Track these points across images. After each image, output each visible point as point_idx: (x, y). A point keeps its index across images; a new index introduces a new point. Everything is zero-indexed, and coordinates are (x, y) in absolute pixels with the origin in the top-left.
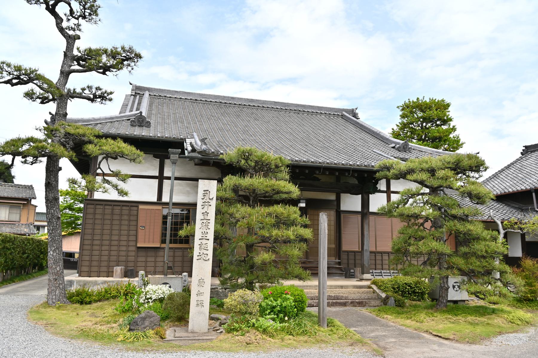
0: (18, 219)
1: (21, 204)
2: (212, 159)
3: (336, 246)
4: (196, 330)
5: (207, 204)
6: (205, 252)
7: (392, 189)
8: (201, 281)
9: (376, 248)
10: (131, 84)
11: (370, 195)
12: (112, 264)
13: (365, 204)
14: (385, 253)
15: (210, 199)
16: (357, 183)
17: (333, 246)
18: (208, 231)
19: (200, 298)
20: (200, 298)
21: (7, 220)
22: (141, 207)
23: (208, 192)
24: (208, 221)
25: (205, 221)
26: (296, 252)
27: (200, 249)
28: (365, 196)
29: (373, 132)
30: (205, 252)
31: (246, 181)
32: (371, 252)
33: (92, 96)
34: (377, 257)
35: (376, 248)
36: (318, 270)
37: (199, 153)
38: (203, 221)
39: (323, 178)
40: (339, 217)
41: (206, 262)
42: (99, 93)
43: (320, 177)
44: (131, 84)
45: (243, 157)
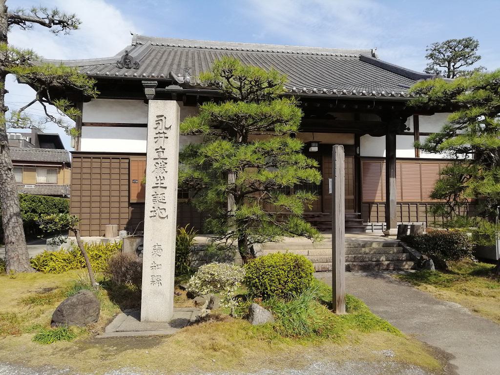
0: (55, 182)
1: (57, 167)
2: (197, 92)
3: (355, 197)
4: (151, 318)
5: (162, 135)
6: (162, 206)
7: (421, 130)
8: (157, 247)
9: (402, 198)
10: (132, 34)
11: (397, 136)
12: (103, 222)
13: (391, 147)
14: (412, 203)
15: (166, 129)
16: (381, 121)
17: (352, 197)
18: (165, 175)
19: (158, 272)
20: (158, 272)
21: (45, 182)
22: (132, 158)
23: (163, 118)
24: (165, 161)
25: (159, 161)
26: (295, 204)
27: (154, 201)
28: (391, 137)
29: (360, 185)
30: (162, 206)
31: (229, 108)
32: (398, 203)
33: (47, 21)
34: (403, 208)
35: (402, 198)
36: (331, 225)
37: (181, 85)
38: (156, 161)
39: (339, 116)
40: (359, 165)
41: (163, 220)
42: (57, 18)
43: (334, 114)
44: (132, 34)
45: (223, 75)
